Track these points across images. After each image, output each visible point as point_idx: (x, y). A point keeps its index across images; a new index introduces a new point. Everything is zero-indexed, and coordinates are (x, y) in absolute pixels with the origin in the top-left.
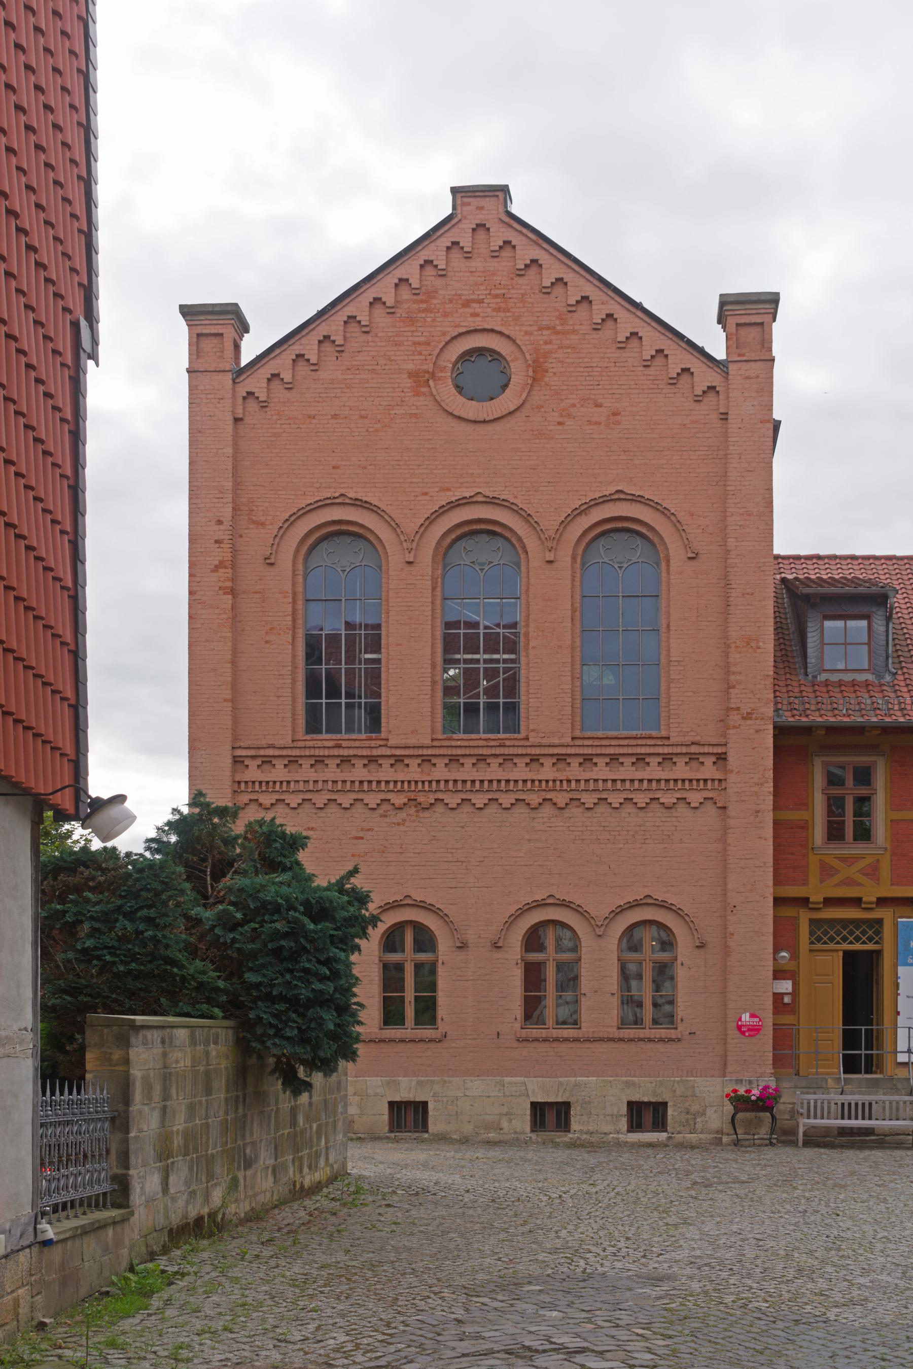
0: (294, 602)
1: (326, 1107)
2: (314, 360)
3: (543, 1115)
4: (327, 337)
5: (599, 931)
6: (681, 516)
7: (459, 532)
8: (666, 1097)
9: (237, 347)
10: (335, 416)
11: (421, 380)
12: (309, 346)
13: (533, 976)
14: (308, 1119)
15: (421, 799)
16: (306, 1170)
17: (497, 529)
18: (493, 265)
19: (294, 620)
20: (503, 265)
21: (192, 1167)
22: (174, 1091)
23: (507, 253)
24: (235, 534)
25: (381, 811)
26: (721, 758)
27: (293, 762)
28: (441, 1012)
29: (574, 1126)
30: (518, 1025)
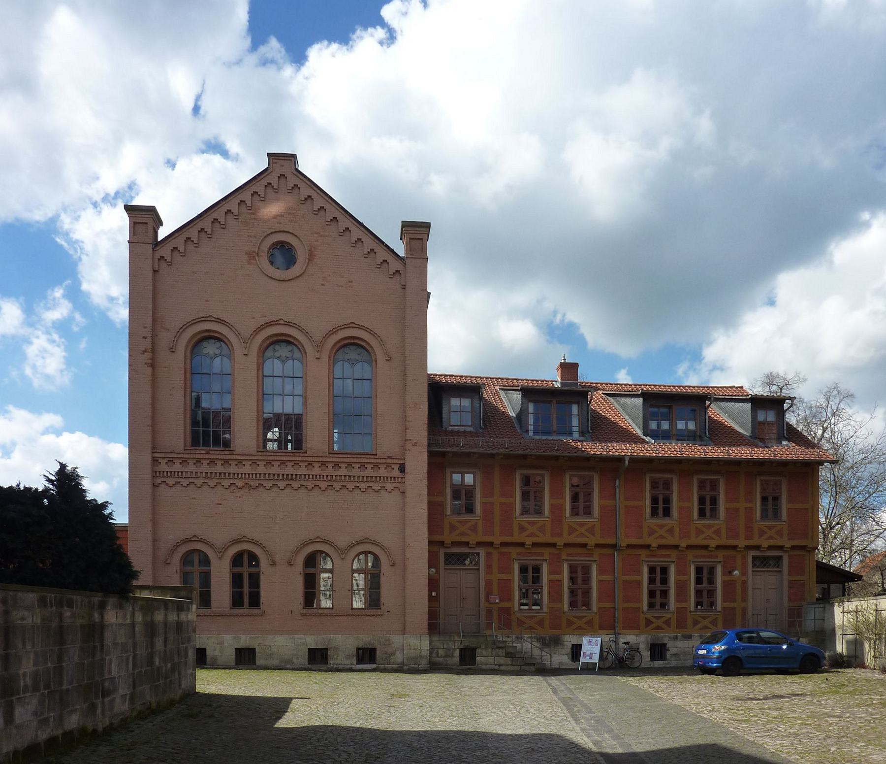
0: (185, 373)
4: (203, 229)
11: (252, 256)
15: (251, 483)
19: (185, 384)
24: (154, 336)
25: (231, 490)
26: (402, 469)
30: (301, 607)
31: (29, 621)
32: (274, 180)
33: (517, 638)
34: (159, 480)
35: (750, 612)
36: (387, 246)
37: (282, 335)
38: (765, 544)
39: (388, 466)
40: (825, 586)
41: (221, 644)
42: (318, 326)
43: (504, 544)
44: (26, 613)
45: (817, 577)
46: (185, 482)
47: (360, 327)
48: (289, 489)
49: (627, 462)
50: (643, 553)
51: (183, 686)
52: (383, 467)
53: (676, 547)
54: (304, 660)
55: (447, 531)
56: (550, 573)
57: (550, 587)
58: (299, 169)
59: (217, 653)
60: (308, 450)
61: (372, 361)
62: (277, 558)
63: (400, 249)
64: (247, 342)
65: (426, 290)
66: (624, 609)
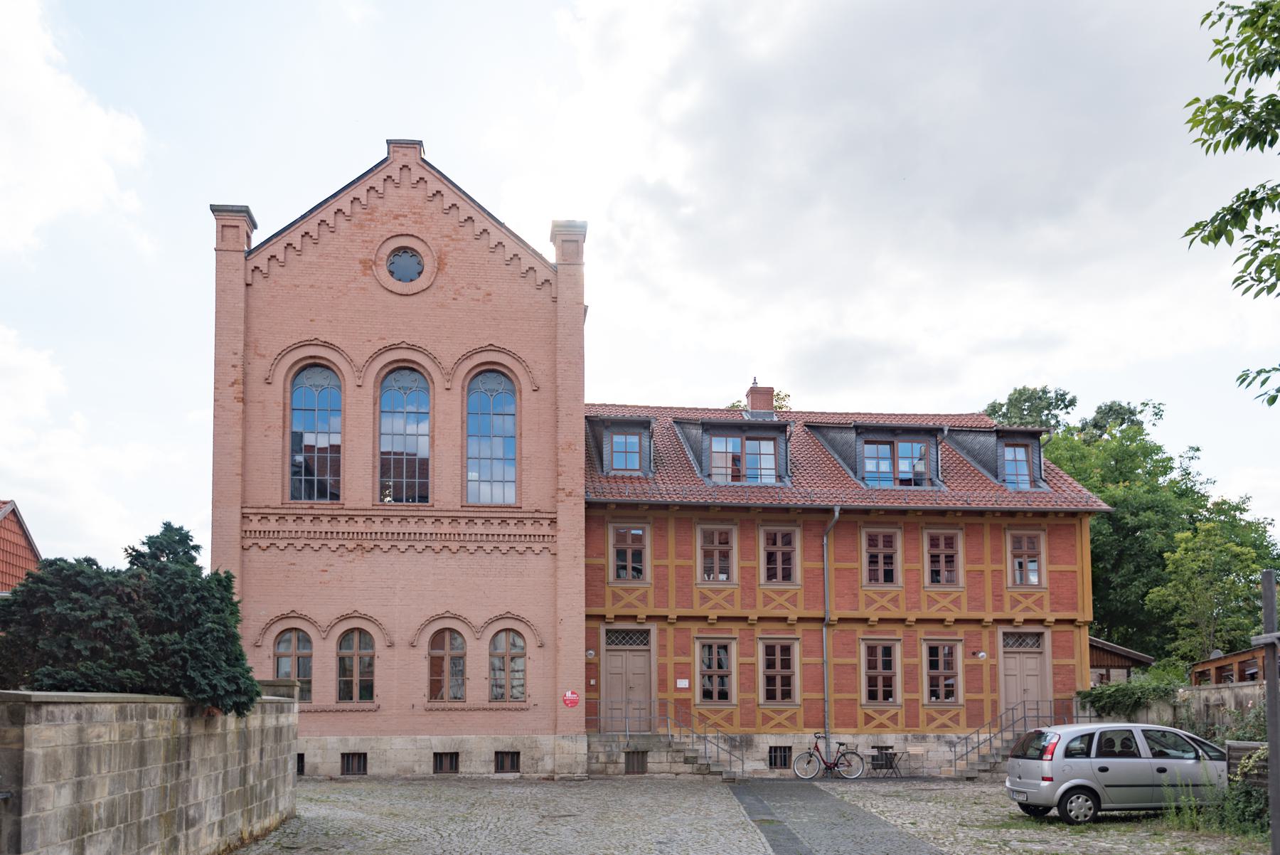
1: (277, 766)
2: (298, 248)
3: (441, 762)
5: (478, 635)
6: (528, 362)
7: (391, 367)
8: (519, 748)
9: (249, 237)
10: (312, 286)
11: (368, 265)
12: (295, 237)
13: (436, 665)
14: (259, 776)
15: (365, 545)
16: (255, 820)
17: (415, 366)
18: (413, 192)
19: (284, 422)
20: (419, 194)
21: (119, 838)
22: (93, 767)
23: (421, 185)
24: (246, 363)
25: (339, 553)
26: (553, 521)
27: (282, 517)
28: (376, 691)
29: (461, 769)
31: (106, 739)
32: (394, 171)
33: (699, 737)
34: (249, 542)
35: (1002, 708)
37: (404, 360)
38: (1020, 618)
39: (536, 521)
40: (1103, 671)
41: (323, 748)
43: (680, 618)
44: (103, 729)
45: (1091, 660)
46: (282, 544)
48: (411, 551)
49: (837, 514)
50: (860, 630)
51: (281, 808)
52: (529, 523)
53: (903, 621)
54: (427, 767)
56: (741, 654)
57: (740, 674)
59: (318, 760)
61: (514, 391)
62: (396, 639)
63: (550, 253)
65: (582, 303)
66: (836, 701)
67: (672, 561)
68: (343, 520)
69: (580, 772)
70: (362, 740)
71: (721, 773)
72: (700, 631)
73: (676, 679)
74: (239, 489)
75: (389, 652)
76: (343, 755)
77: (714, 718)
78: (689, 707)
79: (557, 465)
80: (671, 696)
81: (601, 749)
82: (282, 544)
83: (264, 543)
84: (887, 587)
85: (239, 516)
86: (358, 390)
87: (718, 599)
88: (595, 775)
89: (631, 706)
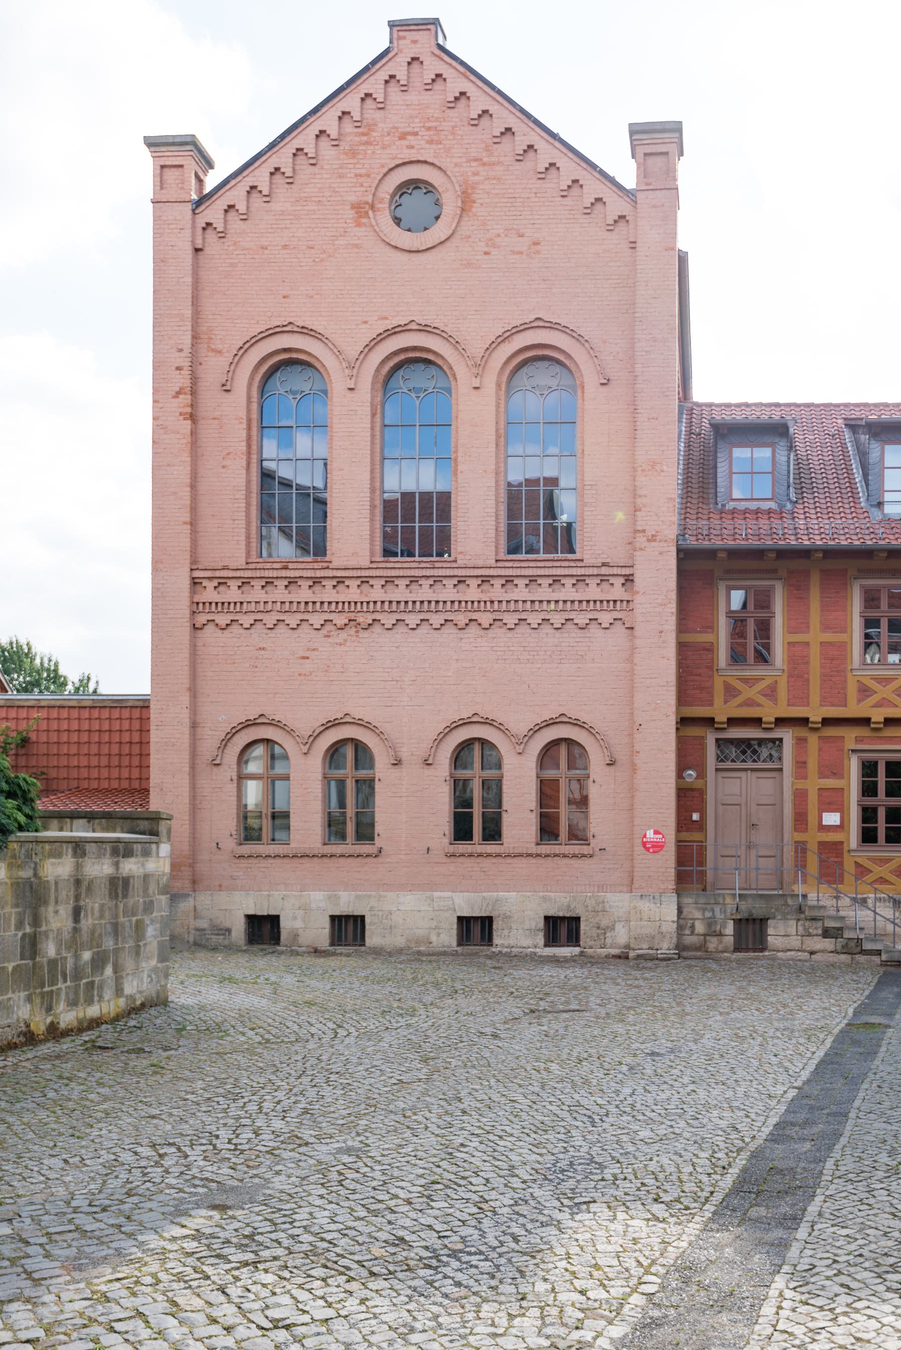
0: (249, 428)
4: (277, 169)
8: (579, 911)
10: (285, 247)
11: (362, 210)
12: (260, 177)
17: (430, 357)
18: (427, 97)
19: (249, 446)
23: (439, 85)
25: (324, 632)
26: (629, 580)
29: (497, 940)
30: (446, 841)
34: (202, 619)
36: (602, 173)
41: (306, 908)
42: (477, 332)
43: (827, 722)
46: (247, 620)
47: (553, 326)
52: (593, 582)
54: (448, 937)
55: (718, 699)
58: (449, 46)
59: (298, 924)
60: (459, 557)
61: (575, 388)
63: (626, 173)
64: (479, 366)
67: (815, 636)
68: (329, 584)
69: (666, 947)
70: (358, 897)
71: (878, 953)
72: (858, 740)
73: (821, 811)
74: (186, 543)
75: (395, 773)
76: (333, 918)
77: (879, 871)
78: (840, 854)
79: (635, 496)
80: (813, 838)
81: (698, 914)
82: (247, 620)
83: (223, 619)
84: (758, 671)
85: (186, 583)
86: (350, 394)
87: (886, 692)
88: (688, 952)
89: (753, 853)
